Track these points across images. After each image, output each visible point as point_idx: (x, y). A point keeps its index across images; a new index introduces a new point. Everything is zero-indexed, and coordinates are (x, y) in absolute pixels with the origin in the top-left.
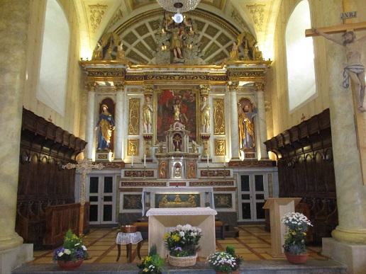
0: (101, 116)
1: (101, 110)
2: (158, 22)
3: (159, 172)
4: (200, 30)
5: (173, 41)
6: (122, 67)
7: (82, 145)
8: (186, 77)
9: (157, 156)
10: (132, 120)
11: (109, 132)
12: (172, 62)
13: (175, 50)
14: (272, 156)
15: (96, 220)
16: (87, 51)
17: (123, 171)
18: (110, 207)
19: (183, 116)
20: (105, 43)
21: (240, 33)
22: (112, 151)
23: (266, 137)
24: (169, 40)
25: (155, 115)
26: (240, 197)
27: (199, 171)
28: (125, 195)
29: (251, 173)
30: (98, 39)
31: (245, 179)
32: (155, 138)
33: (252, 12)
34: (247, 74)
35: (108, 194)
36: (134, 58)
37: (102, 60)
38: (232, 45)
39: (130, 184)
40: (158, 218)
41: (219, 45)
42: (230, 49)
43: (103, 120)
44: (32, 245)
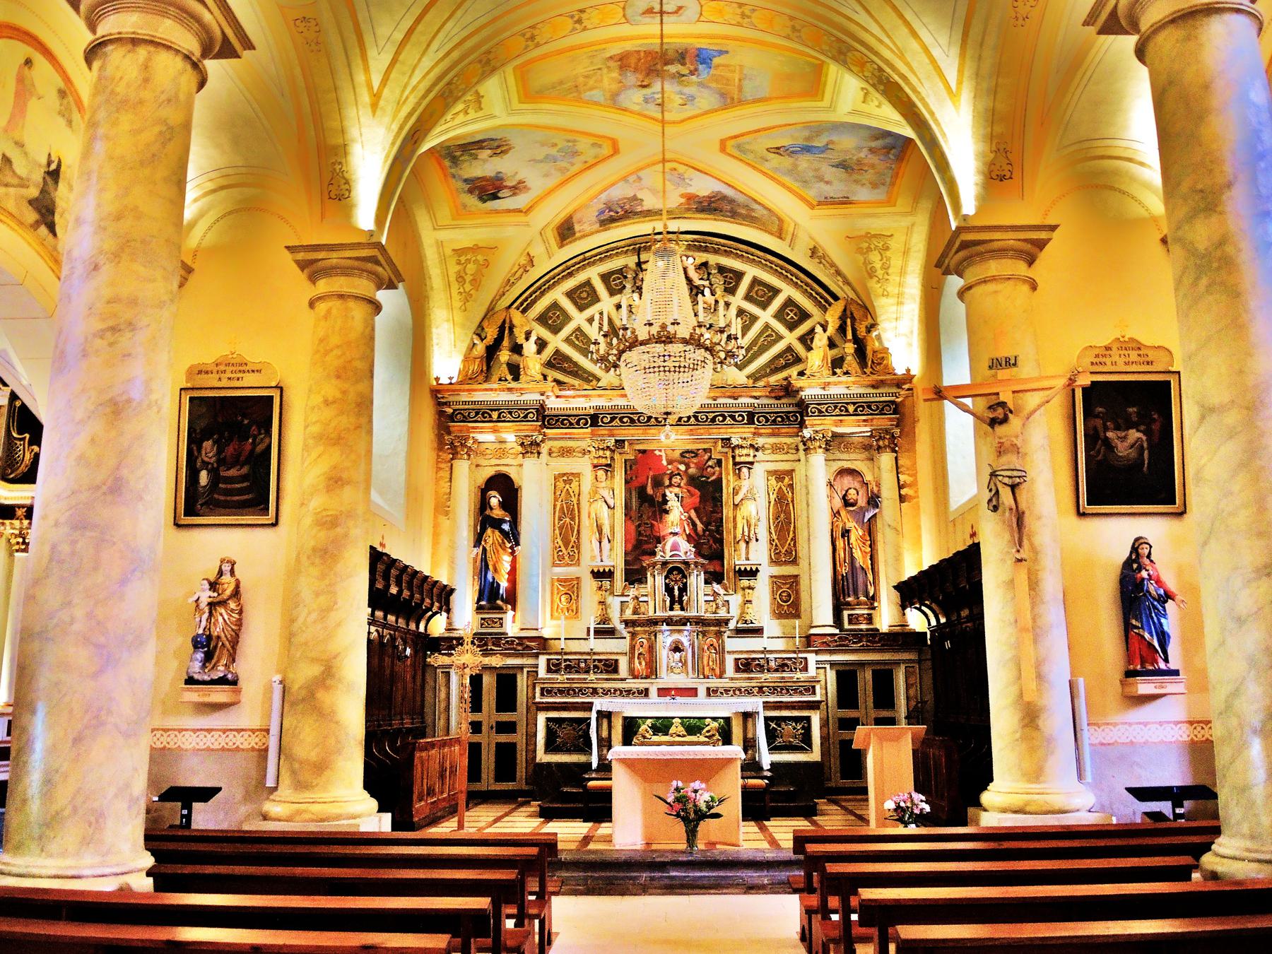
0: (485, 521)
1: (484, 504)
2: (621, 272)
3: (631, 661)
4: (731, 291)
6: (538, 397)
7: (444, 595)
9: (627, 623)
10: (561, 528)
11: (506, 559)
14: (917, 621)
16: (447, 361)
18: (512, 747)
19: (690, 518)
20: (491, 333)
22: (514, 609)
23: (898, 571)
25: (620, 513)
26: (521, 728)
28: (548, 719)
29: (862, 664)
31: (846, 677)
32: (619, 576)
34: (851, 408)
35: (506, 717)
37: (487, 379)
39: (561, 692)
40: (629, 763)
41: (781, 329)
42: (807, 340)
43: (489, 531)
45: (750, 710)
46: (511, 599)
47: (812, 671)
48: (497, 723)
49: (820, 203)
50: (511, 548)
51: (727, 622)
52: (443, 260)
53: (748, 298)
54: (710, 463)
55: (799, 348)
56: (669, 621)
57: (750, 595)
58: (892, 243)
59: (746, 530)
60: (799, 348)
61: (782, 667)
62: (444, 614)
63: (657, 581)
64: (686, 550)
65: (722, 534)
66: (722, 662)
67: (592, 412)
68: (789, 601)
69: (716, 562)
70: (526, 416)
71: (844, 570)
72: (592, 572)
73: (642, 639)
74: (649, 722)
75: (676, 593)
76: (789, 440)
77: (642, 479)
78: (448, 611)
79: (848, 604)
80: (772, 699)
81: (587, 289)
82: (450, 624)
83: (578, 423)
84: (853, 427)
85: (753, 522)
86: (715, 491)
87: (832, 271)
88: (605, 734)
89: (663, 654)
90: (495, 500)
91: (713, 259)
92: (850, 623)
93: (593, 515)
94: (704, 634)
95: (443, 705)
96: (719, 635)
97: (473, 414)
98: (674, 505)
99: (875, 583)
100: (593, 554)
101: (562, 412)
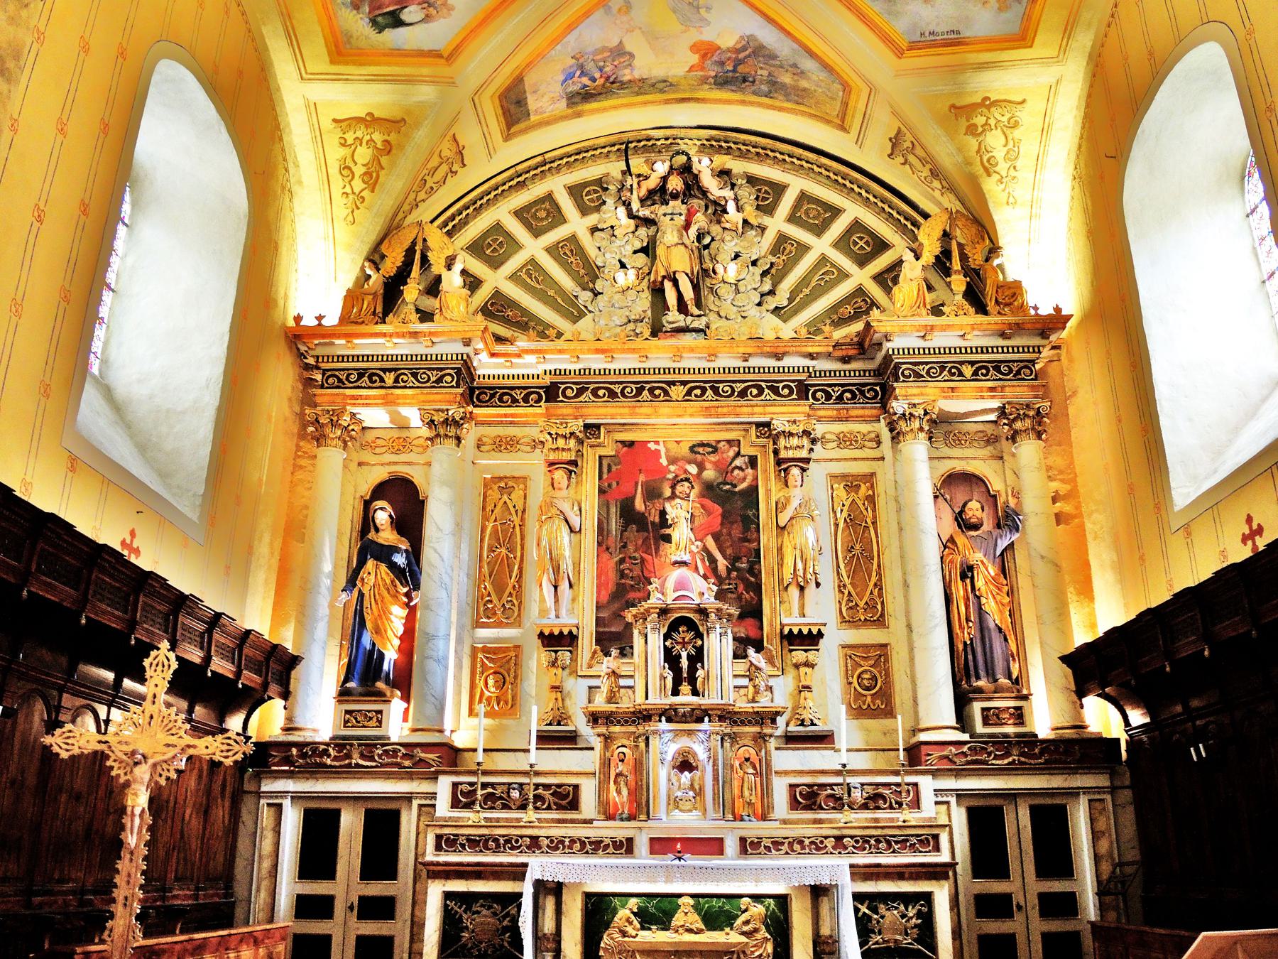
1: (367, 523)
3: (602, 789)
4: (769, 210)
5: (660, 251)
6: (459, 348)
8: (716, 391)
9: (594, 718)
11: (398, 614)
12: (656, 331)
13: (668, 285)
14: (1103, 718)
15: (1118, 740)
16: (319, 277)
17: (443, 786)
19: (705, 549)
21: (926, 216)
22: (406, 698)
24: (648, 250)
25: (590, 539)
26: (404, 910)
27: (780, 790)
28: (448, 896)
29: (1012, 796)
30: (365, 249)
31: (986, 821)
32: (587, 642)
33: (972, 130)
35: (376, 888)
36: (507, 322)
38: (899, 263)
39: (475, 843)
42: (888, 278)
43: (371, 564)
44: (1148, 720)
45: (825, 881)
46: (403, 681)
47: (929, 809)
48: (361, 899)
49: (914, 46)
50: (408, 595)
51: (773, 717)
52: (318, 136)
53: (792, 219)
54: (738, 462)
55: (876, 291)
56: (670, 715)
57: (808, 676)
58: (1023, 115)
59: (800, 566)
60: (876, 291)
61: (874, 800)
62: (278, 703)
63: (650, 645)
64: (701, 591)
65: (758, 576)
66: (767, 792)
67: (547, 380)
68: (874, 692)
69: (750, 621)
70: (440, 380)
71: (967, 633)
72: (541, 635)
73: (624, 746)
74: (633, 903)
75: (684, 663)
76: (864, 428)
77: (626, 488)
78: (286, 695)
79: (980, 690)
80: (863, 859)
81: (547, 205)
82: (289, 719)
83: (526, 399)
84: (974, 402)
85: (810, 554)
86: (746, 507)
87: (926, 173)
88: (548, 926)
89: (661, 776)
90: (382, 517)
91: (739, 167)
92: (986, 722)
93: (544, 542)
94: (734, 738)
95: (266, 864)
96: (761, 739)
97: (354, 377)
98: (681, 532)
99: (1021, 656)
100: (544, 607)
101: (502, 382)
